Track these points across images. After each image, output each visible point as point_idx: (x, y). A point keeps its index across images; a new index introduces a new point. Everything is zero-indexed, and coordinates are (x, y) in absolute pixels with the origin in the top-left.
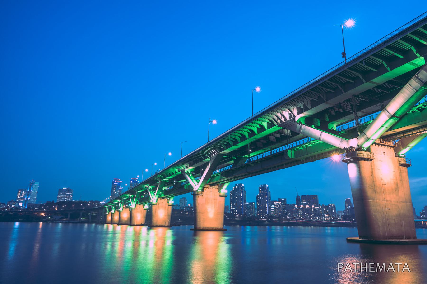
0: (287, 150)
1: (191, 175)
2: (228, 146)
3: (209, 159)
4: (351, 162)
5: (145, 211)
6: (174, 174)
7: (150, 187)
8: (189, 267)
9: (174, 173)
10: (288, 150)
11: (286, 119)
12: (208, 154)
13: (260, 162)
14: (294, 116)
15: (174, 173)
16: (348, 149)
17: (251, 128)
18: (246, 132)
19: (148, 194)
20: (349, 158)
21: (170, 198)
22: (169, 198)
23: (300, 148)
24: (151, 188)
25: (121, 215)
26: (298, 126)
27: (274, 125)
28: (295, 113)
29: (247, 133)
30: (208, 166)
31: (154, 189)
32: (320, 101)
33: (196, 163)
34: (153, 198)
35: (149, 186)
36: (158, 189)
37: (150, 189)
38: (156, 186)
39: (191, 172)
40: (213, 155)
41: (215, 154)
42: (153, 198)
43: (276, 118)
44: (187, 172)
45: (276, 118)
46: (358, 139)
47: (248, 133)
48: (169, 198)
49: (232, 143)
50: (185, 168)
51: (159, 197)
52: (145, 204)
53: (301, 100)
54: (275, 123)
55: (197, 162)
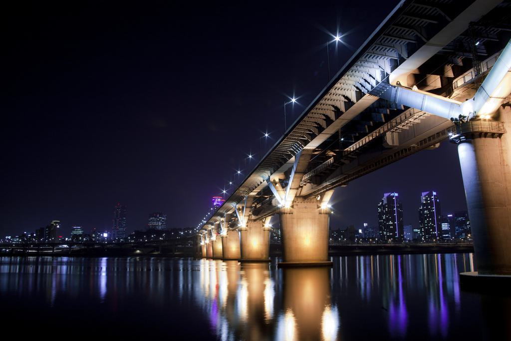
0: (385, 133)
1: (277, 185)
2: (313, 136)
3: (293, 159)
4: (461, 142)
5: (325, 220)
6: (332, 122)
7: (276, 177)
8: (329, 297)
9: (332, 116)
10: (387, 133)
11: (372, 87)
12: (291, 151)
13: (356, 157)
14: (388, 75)
15: (332, 116)
16: (458, 119)
17: (334, 102)
18: (321, 114)
19: (237, 215)
20: (457, 135)
21: (322, 195)
22: (319, 198)
23: (403, 128)
24: (277, 180)
25: (214, 246)
26: (394, 90)
27: (364, 94)
28: (388, 69)
29: (332, 112)
30: (293, 170)
31: (284, 184)
32: (431, 32)
33: (453, 19)
34: (282, 199)
35: (271, 174)
36: (296, 173)
37: (239, 208)
38: (287, 174)
39: (279, 179)
40: (297, 152)
41: (299, 150)
42: (282, 199)
43: (362, 82)
44: (272, 180)
45: (362, 82)
46: (474, 99)
47: (324, 119)
48: (319, 198)
49: (317, 130)
50: (270, 175)
51: (249, 220)
52: (265, 218)
53: (389, 45)
54: (363, 90)
55: (281, 164)
